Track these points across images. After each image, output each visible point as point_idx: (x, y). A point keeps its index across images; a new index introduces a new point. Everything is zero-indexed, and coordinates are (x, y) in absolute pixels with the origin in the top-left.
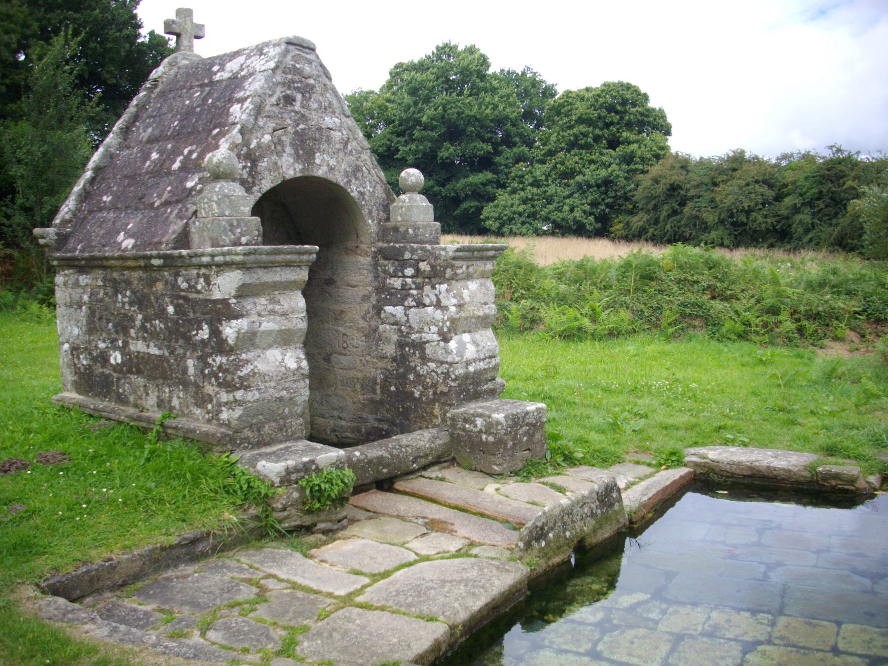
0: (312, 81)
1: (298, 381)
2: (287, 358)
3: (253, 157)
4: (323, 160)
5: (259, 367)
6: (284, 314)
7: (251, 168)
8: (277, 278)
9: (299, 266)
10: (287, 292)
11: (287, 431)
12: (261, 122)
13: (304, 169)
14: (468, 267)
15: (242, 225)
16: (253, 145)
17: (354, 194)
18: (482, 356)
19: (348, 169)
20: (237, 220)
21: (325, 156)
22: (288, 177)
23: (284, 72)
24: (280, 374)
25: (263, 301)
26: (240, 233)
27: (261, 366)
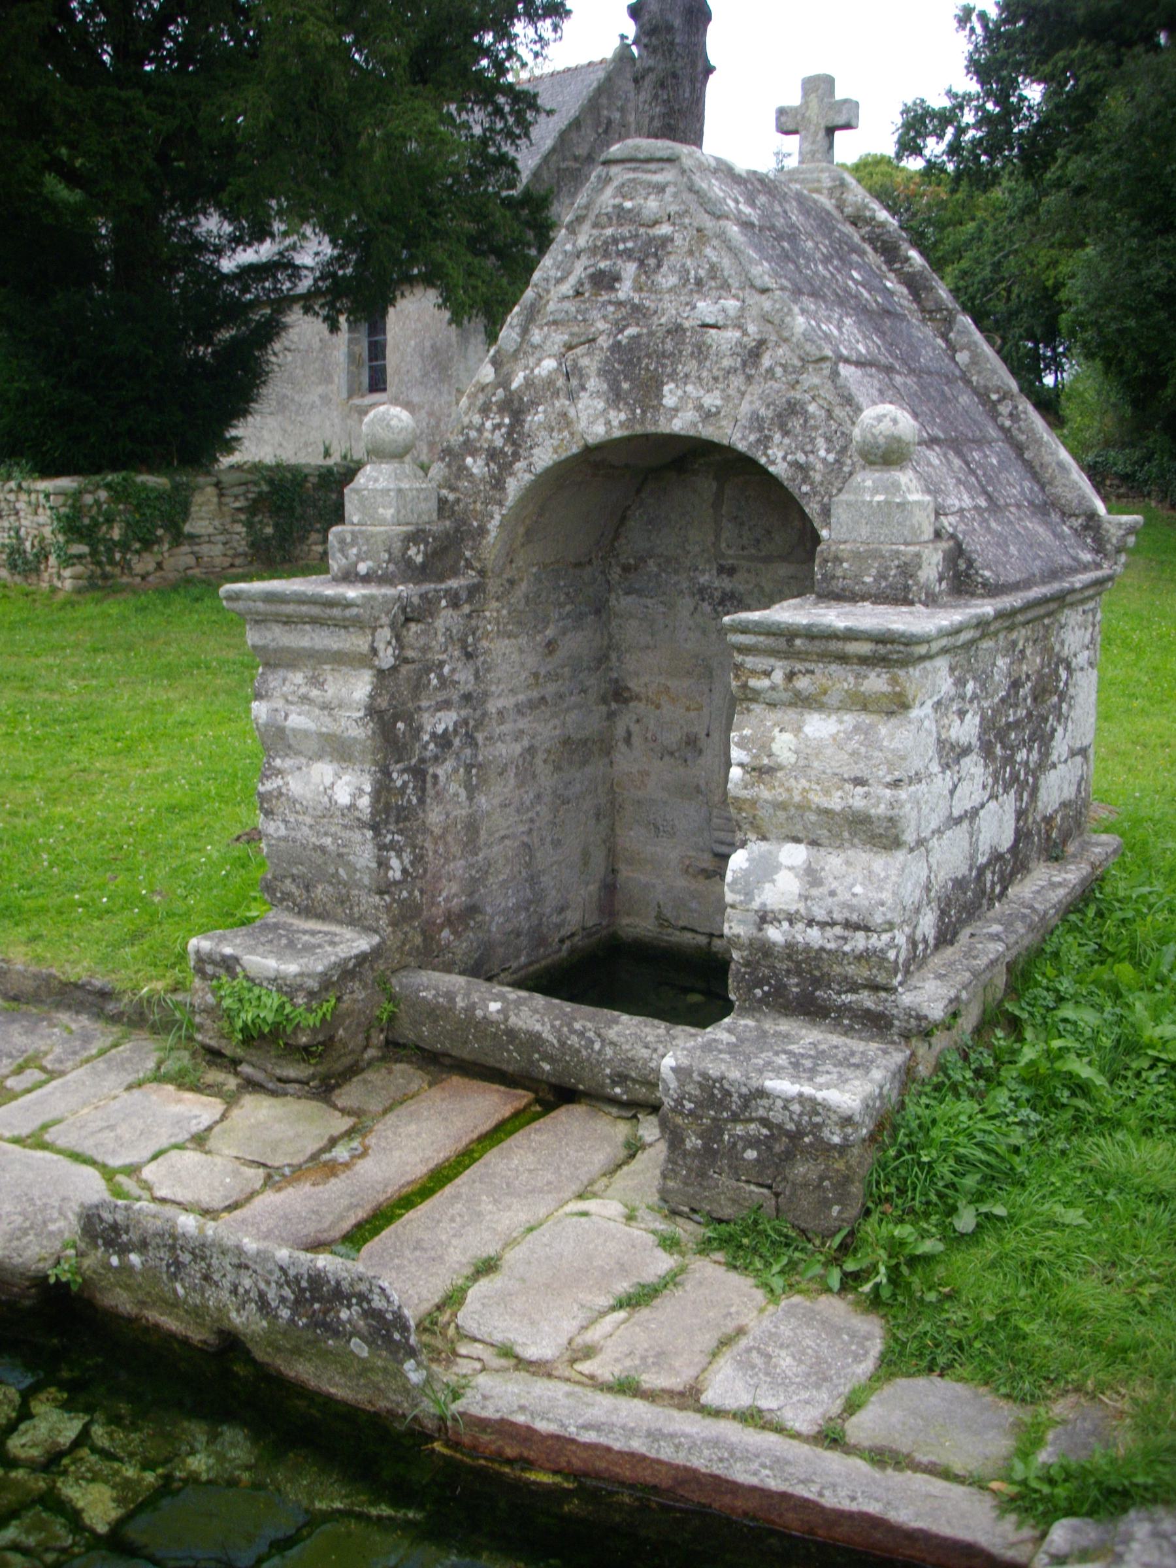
0: (665, 229)
1: (351, 828)
2: (340, 782)
3: (516, 404)
4: (685, 396)
5: (292, 785)
6: (325, 707)
7: (511, 427)
8: (305, 643)
9: (345, 627)
10: (344, 669)
11: (351, 909)
12: (536, 336)
13: (631, 420)
14: (790, 676)
15: (360, 541)
16: (517, 382)
17: (779, 469)
18: (820, 915)
19: (762, 412)
20: (353, 533)
21: (690, 388)
22: (591, 440)
23: (595, 225)
24: (320, 807)
25: (298, 677)
26: (357, 555)
27: (295, 786)
